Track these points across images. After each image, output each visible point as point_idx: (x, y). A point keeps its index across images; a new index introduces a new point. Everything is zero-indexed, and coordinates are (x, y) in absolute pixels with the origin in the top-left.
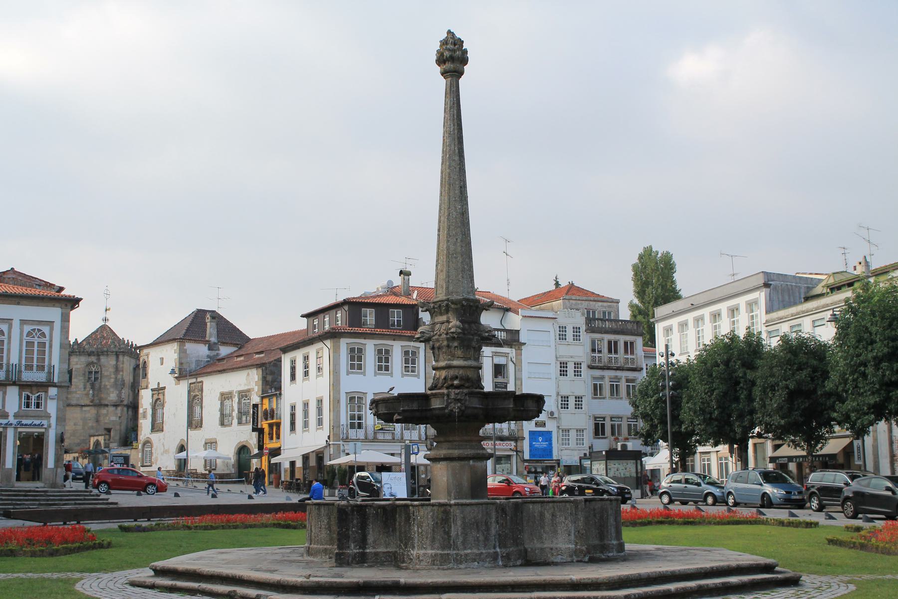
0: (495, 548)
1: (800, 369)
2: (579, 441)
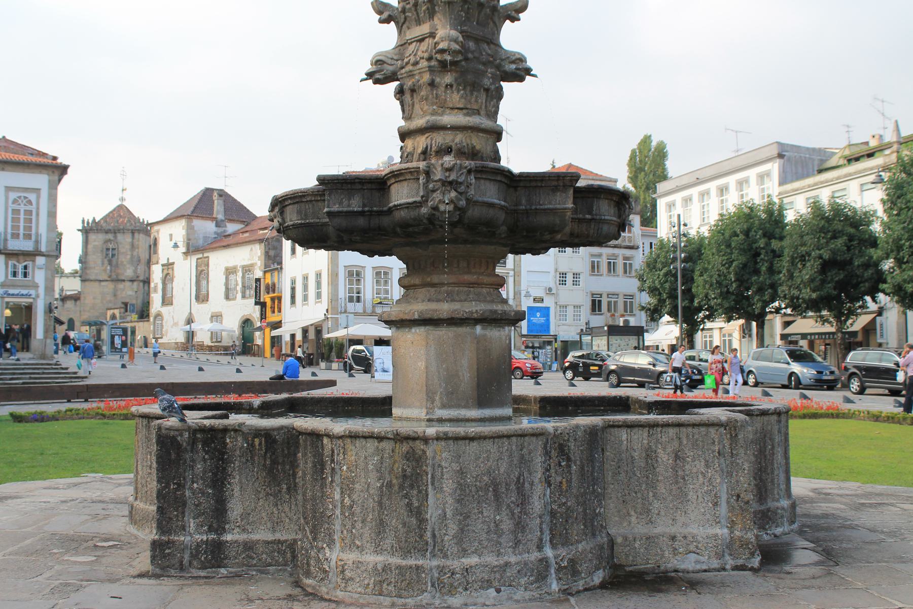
0: (540, 548)
1: (834, 237)
2: (577, 317)
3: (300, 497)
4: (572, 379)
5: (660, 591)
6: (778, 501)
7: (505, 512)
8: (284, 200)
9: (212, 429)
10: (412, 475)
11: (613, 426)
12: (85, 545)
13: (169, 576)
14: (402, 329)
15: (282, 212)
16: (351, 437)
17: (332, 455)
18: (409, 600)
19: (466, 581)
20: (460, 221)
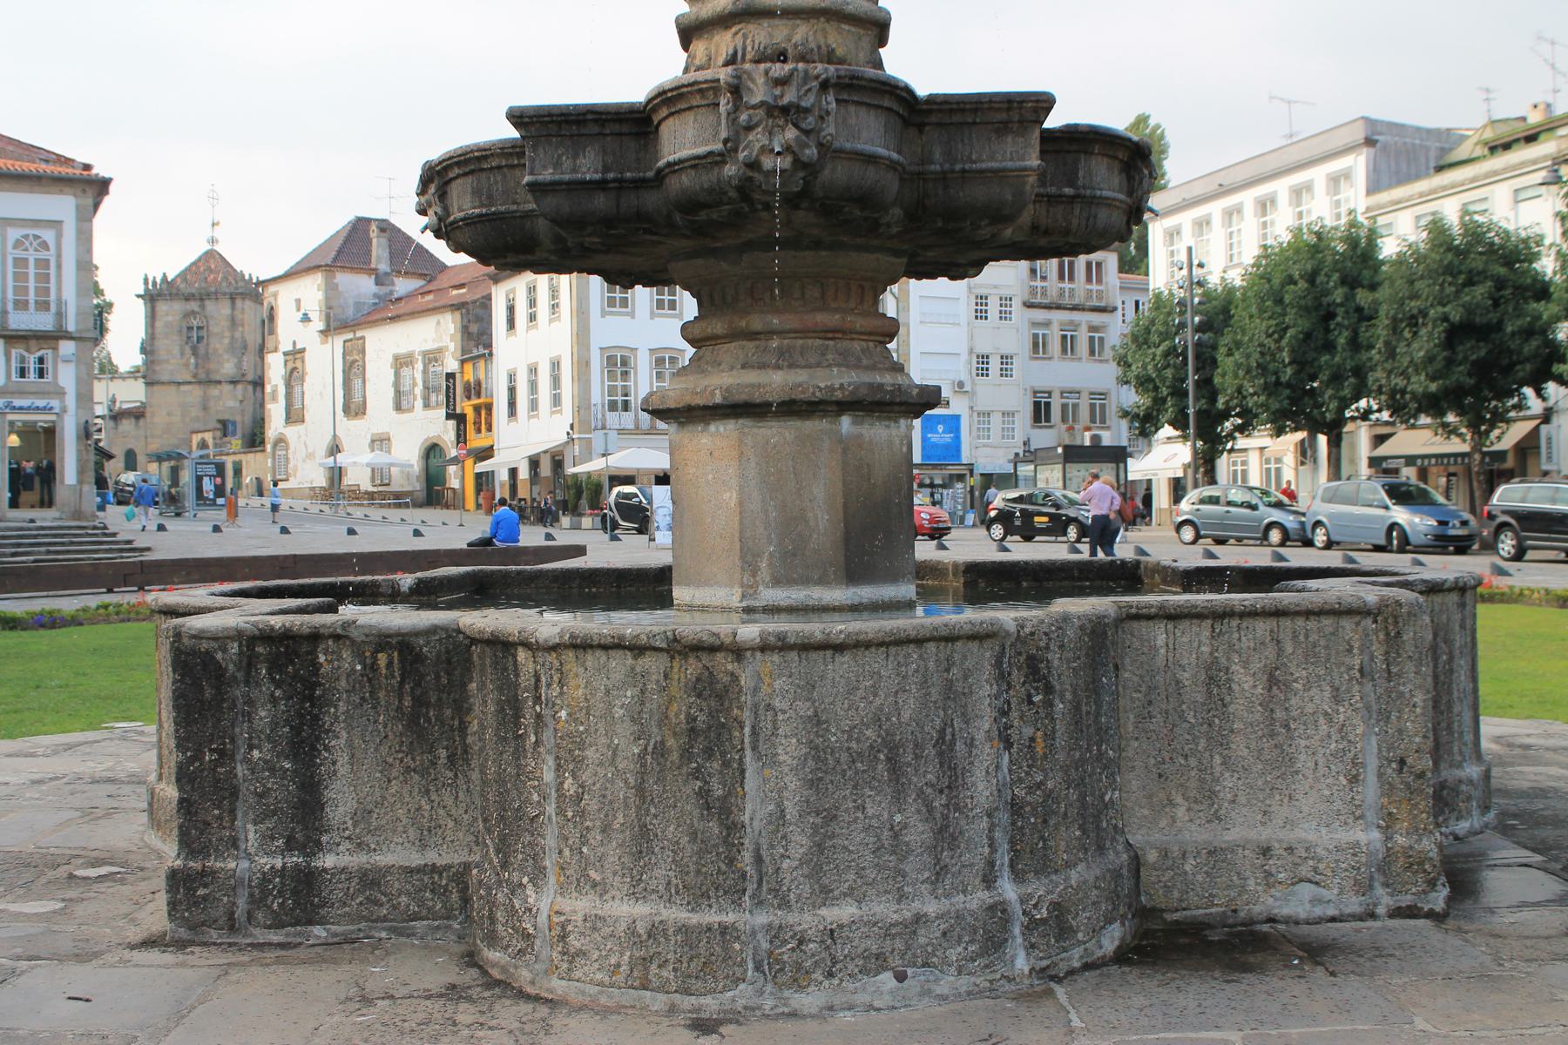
0: (989, 881)
1: (1470, 282)
2: (1007, 432)
3: (475, 775)
4: (1003, 539)
5: (1247, 968)
6: (1460, 766)
7: (912, 805)
8: (446, 169)
9: (286, 638)
10: (710, 728)
11: (1137, 617)
12: (51, 874)
13: (205, 944)
14: (691, 427)
15: (442, 195)
16: (575, 647)
17: (537, 687)
18: (707, 1000)
19: (831, 957)
20: (805, 193)
